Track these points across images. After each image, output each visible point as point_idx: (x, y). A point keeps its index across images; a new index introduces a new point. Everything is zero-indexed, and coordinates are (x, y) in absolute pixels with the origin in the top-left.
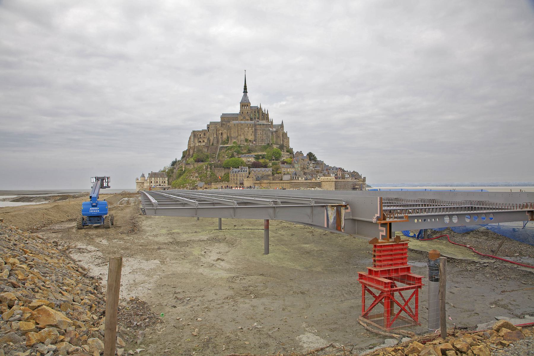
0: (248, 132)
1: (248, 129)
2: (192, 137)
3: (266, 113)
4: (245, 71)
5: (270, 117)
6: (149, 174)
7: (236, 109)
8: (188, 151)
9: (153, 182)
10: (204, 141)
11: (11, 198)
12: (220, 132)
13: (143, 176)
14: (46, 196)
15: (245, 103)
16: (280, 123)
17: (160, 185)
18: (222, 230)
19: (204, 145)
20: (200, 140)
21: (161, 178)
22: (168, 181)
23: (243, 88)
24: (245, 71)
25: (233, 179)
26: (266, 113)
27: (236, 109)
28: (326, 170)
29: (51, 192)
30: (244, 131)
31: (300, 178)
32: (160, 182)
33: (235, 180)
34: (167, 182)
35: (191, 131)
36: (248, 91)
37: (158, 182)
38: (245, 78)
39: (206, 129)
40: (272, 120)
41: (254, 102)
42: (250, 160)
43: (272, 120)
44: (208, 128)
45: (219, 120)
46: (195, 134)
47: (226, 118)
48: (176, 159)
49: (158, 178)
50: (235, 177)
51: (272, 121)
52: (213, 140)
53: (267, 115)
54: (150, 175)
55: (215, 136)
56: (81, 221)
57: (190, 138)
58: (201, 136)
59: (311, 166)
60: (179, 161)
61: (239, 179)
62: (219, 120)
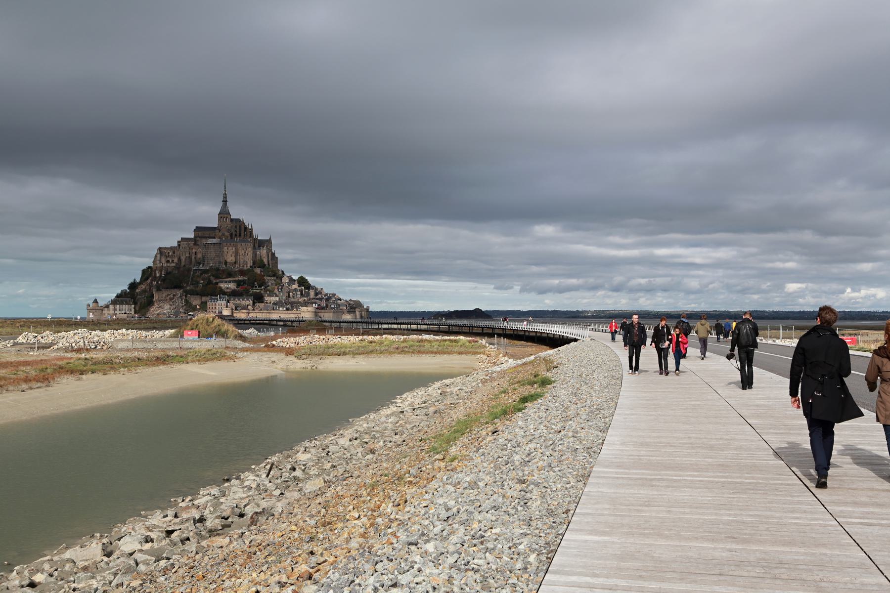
2: (159, 256)
3: (250, 228)
9: (118, 310)
17: (125, 313)
19: (174, 266)
20: (168, 259)
22: (135, 308)
34: (133, 310)
42: (230, 286)
44: (179, 245)
48: (135, 281)
50: (214, 307)
53: (251, 229)
55: (187, 255)
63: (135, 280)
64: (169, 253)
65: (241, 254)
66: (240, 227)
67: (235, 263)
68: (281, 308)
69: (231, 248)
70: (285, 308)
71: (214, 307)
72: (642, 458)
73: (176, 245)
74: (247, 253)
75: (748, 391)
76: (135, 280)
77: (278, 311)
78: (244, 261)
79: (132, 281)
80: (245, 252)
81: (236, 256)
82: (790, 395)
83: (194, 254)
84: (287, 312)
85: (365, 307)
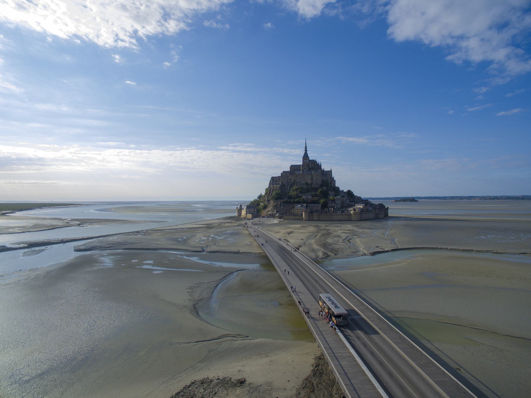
1: (308, 176)
2: (271, 181)
7: (299, 162)
8: (317, 333)
10: (279, 184)
11: (187, 228)
12: (290, 178)
14: (47, 151)
15: (306, 156)
16: (330, 170)
19: (279, 187)
20: (276, 183)
23: (305, 148)
26: (320, 164)
27: (299, 162)
28: (359, 200)
31: (338, 211)
35: (271, 177)
36: (307, 149)
39: (280, 175)
41: (312, 156)
45: (288, 170)
46: (273, 179)
47: (294, 168)
50: (298, 211)
55: (286, 180)
57: (270, 182)
59: (348, 202)
62: (288, 170)
67: (312, 184)
73: (280, 175)
81: (312, 181)
82: (284, 172)
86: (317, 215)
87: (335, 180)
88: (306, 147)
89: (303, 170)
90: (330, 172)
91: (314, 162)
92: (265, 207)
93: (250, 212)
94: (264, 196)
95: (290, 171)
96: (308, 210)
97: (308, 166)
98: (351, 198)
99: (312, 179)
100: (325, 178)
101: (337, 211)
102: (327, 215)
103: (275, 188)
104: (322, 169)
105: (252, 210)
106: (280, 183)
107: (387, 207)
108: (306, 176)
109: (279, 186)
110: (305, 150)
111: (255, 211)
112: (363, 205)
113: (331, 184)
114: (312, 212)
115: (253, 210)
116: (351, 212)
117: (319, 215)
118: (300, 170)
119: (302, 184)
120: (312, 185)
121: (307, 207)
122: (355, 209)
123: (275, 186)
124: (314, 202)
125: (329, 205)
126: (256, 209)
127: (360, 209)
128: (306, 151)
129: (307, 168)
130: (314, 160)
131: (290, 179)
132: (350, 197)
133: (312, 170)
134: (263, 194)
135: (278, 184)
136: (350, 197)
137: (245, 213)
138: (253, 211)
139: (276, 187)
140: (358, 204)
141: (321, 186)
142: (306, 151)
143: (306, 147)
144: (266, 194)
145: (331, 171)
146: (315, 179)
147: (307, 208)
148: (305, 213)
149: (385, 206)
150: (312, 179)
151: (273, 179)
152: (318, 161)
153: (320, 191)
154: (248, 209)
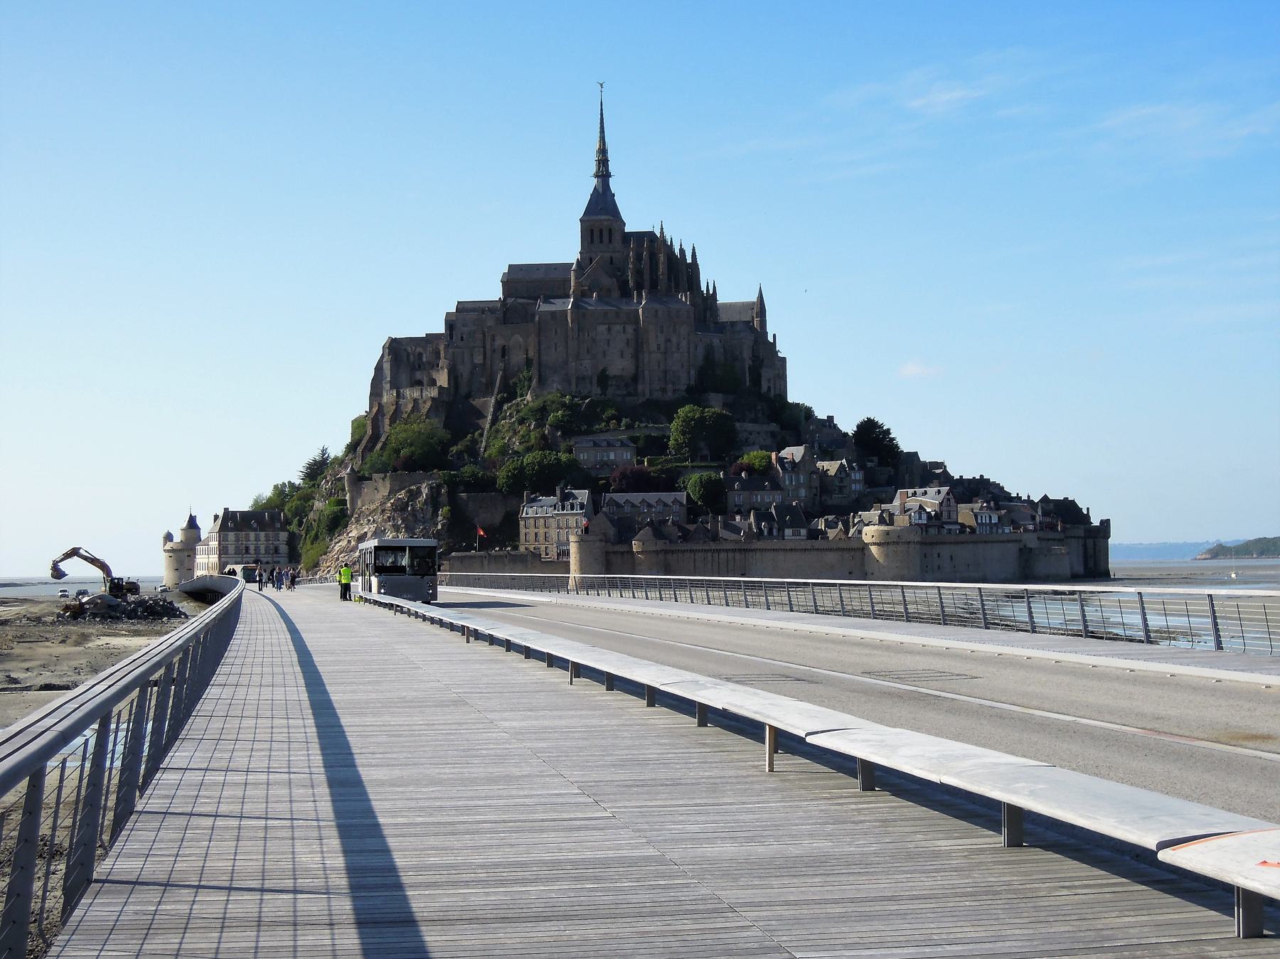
0: (609, 344)
1: (609, 329)
3: (689, 260)
4: (601, 85)
5: (706, 278)
6: (216, 517)
10: (433, 382)
12: (499, 342)
13: (192, 523)
18: (279, 553)
19: (433, 399)
21: (262, 534)
24: (601, 85)
25: (532, 537)
26: (689, 260)
29: (917, 624)
30: (594, 340)
31: (788, 532)
32: (257, 549)
33: (541, 538)
37: (252, 551)
38: (602, 114)
39: (440, 328)
40: (714, 287)
41: (635, 220)
42: (612, 456)
43: (714, 287)
45: (494, 293)
46: (396, 348)
48: (324, 455)
49: (252, 535)
50: (541, 531)
51: (711, 292)
52: (472, 373)
53: (694, 266)
54: (219, 521)
55: (478, 359)
56: (259, 604)
57: (379, 368)
58: (424, 359)
59: (856, 481)
60: (336, 458)
61: (555, 537)
62: (494, 293)
63: (324, 452)
64: (420, 355)
65: (653, 347)
66: (653, 257)
67: (635, 379)
68: (788, 532)
69: (618, 328)
70: (803, 532)
71: (541, 531)
72: (462, 731)
73: (440, 328)
74: (674, 340)
75: (830, 415)
76: (324, 452)
77: (775, 543)
78: (665, 372)
79: (313, 454)
80: (669, 340)
81: (636, 356)
82: (462, 307)
83: (498, 355)
84: (809, 544)
85: (1095, 522)
86: (657, 552)
87: (784, 360)
88: (603, 151)
89: (582, 295)
90: (830, 418)
91: (652, 243)
92: (338, 522)
93: (247, 549)
94: (340, 462)
95: (503, 302)
96: (601, 520)
97: (616, 269)
98: (880, 464)
99: (638, 346)
100: (716, 342)
101: (781, 530)
102: (718, 551)
103: (410, 406)
104: (704, 288)
105: (257, 539)
106: (443, 379)
107: (1102, 522)
108: (602, 328)
109: (434, 393)
110: (596, 176)
111: (276, 550)
112: (939, 492)
113: (757, 380)
114: (625, 529)
115: (268, 540)
116: (865, 529)
117: (666, 552)
118: (568, 297)
119: (574, 381)
120: (640, 387)
121: (595, 507)
122: (891, 515)
123: (410, 393)
124: (638, 482)
125: (737, 497)
126: (283, 536)
127: (924, 516)
128: (603, 173)
129: (607, 281)
130: (652, 234)
131: (504, 351)
132: (875, 459)
133: (640, 296)
134: (337, 449)
135: (425, 380)
136: (875, 459)
137: (214, 559)
138: (267, 552)
139: (415, 401)
140: (911, 491)
141: (695, 394)
142: (603, 173)
143: (603, 151)
144: (352, 448)
145: (759, 308)
146: (653, 347)
147: (596, 511)
148: (581, 542)
149: (1087, 516)
150: (638, 346)
151: (396, 348)
152: (681, 237)
153: (687, 421)
154: (231, 535)
